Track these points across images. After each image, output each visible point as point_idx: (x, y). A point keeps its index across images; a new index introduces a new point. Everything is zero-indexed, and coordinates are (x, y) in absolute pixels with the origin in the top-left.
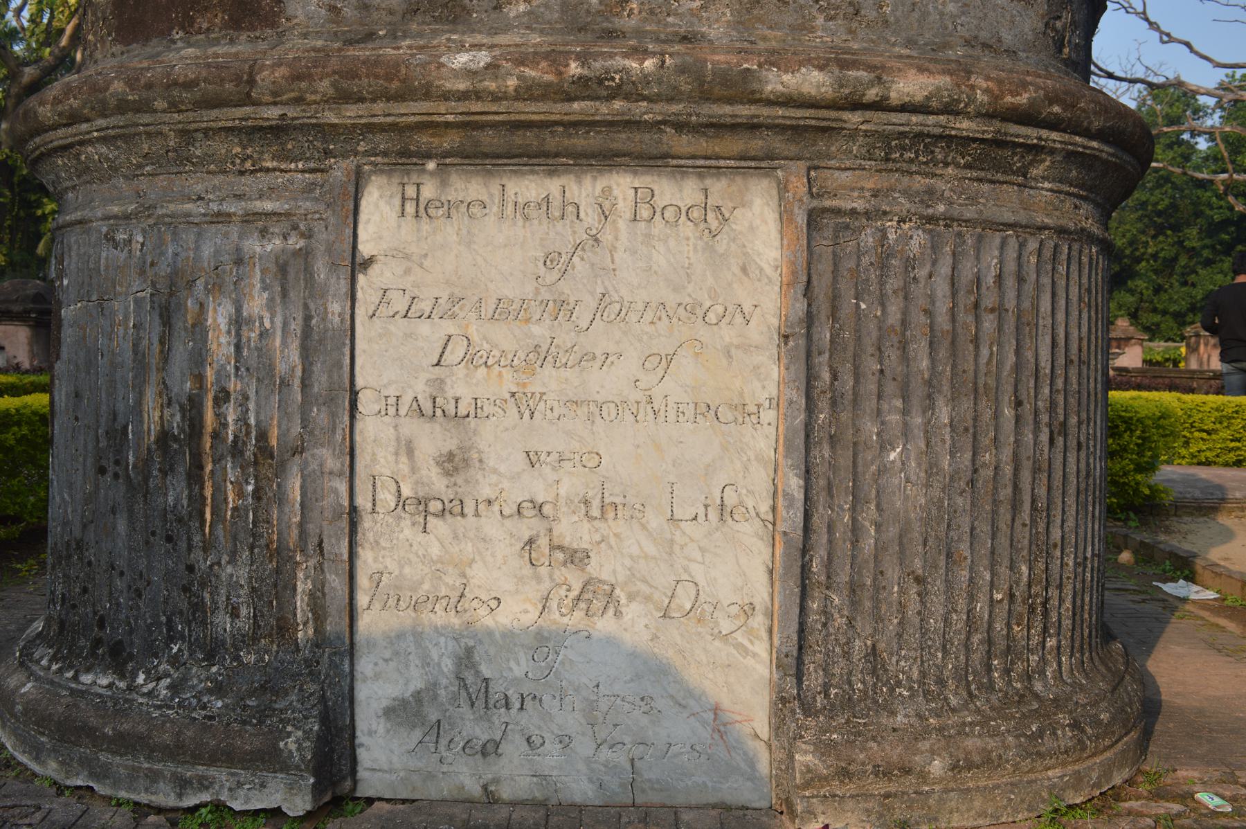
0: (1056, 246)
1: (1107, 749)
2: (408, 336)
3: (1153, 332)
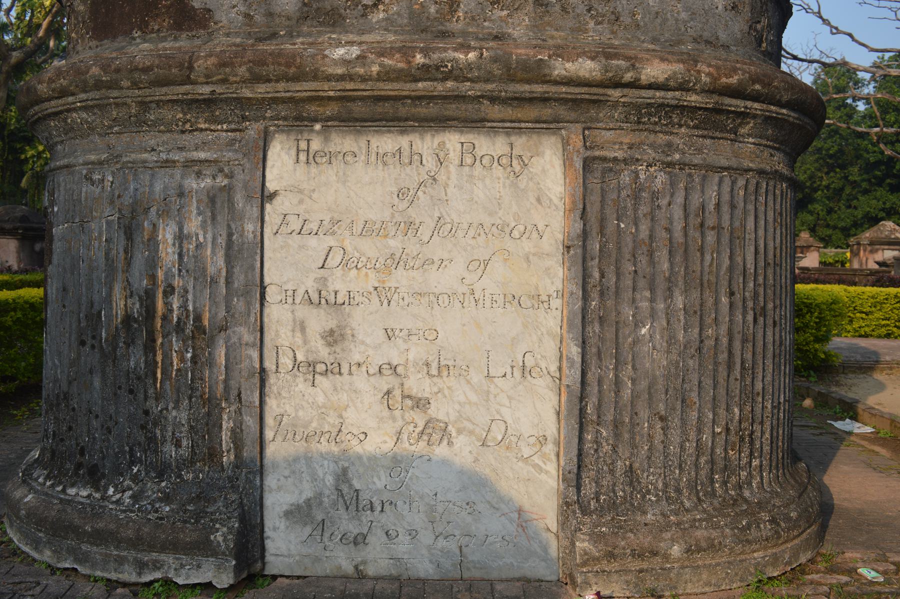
0: (758, 183)
1: (795, 537)
2: (301, 247)
3: (827, 242)
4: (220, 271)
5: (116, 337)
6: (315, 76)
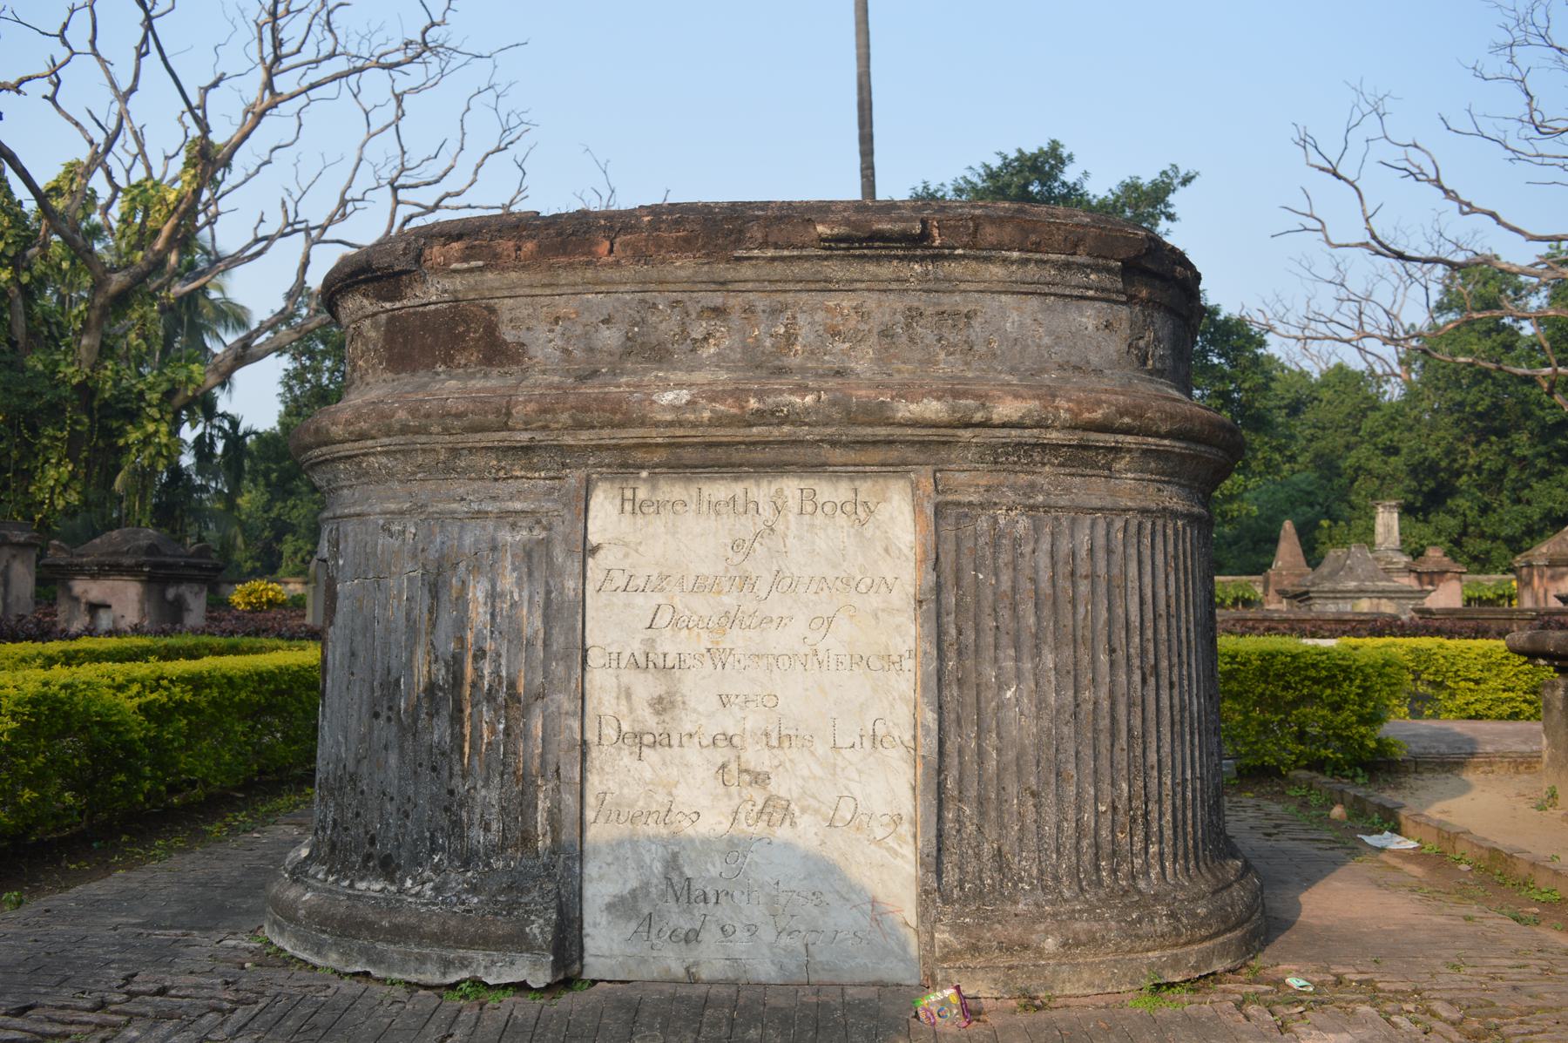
0: (1140, 524)
1: (1204, 939)
2: (628, 605)
3: (1482, 563)
4: (536, 632)
5: (417, 707)
6: (642, 422)
